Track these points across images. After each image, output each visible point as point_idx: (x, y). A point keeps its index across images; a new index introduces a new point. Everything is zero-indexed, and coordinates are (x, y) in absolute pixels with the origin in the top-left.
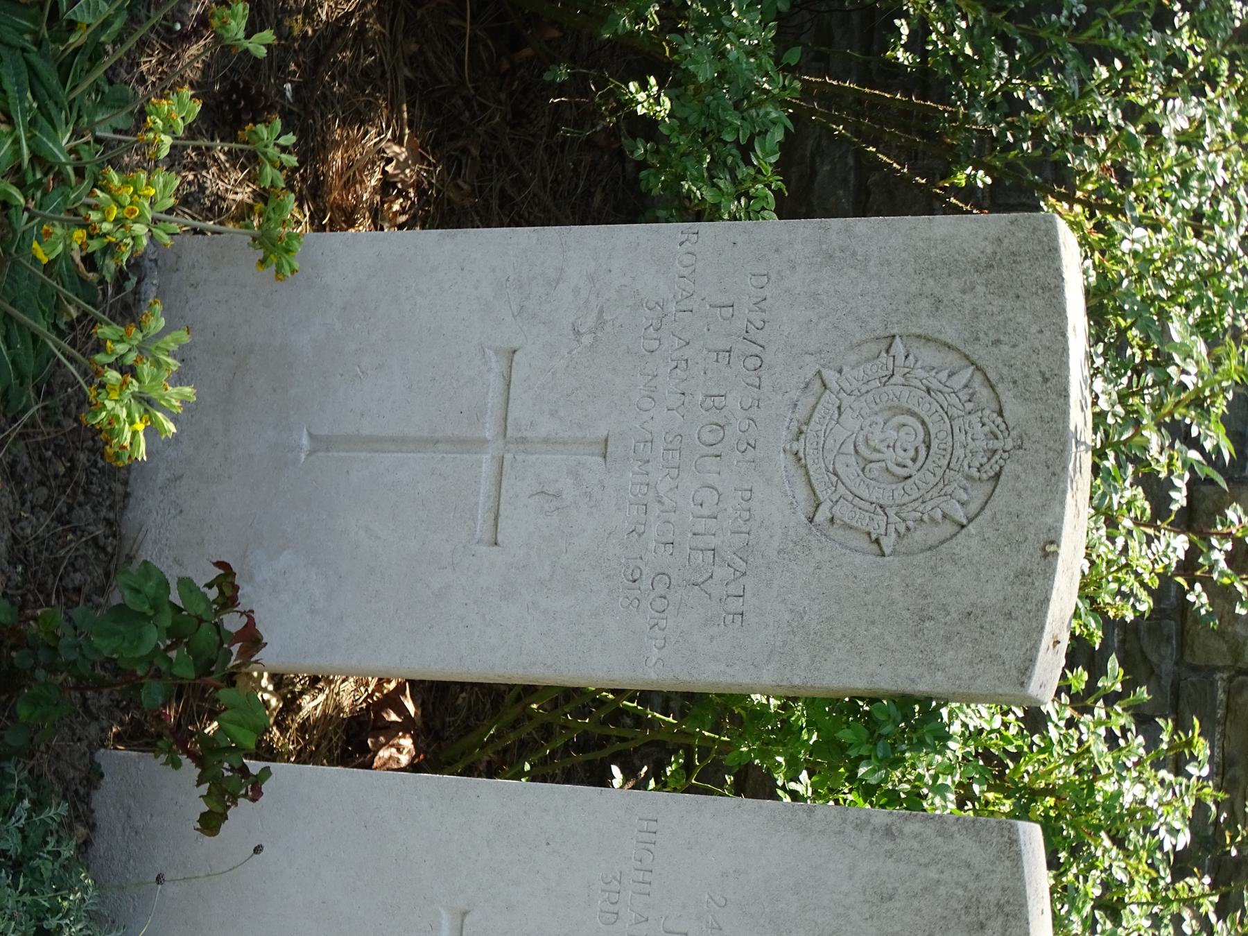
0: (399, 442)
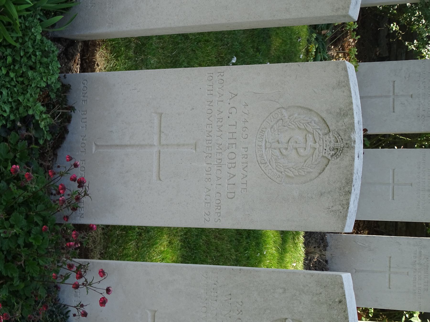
0: (376, 97)
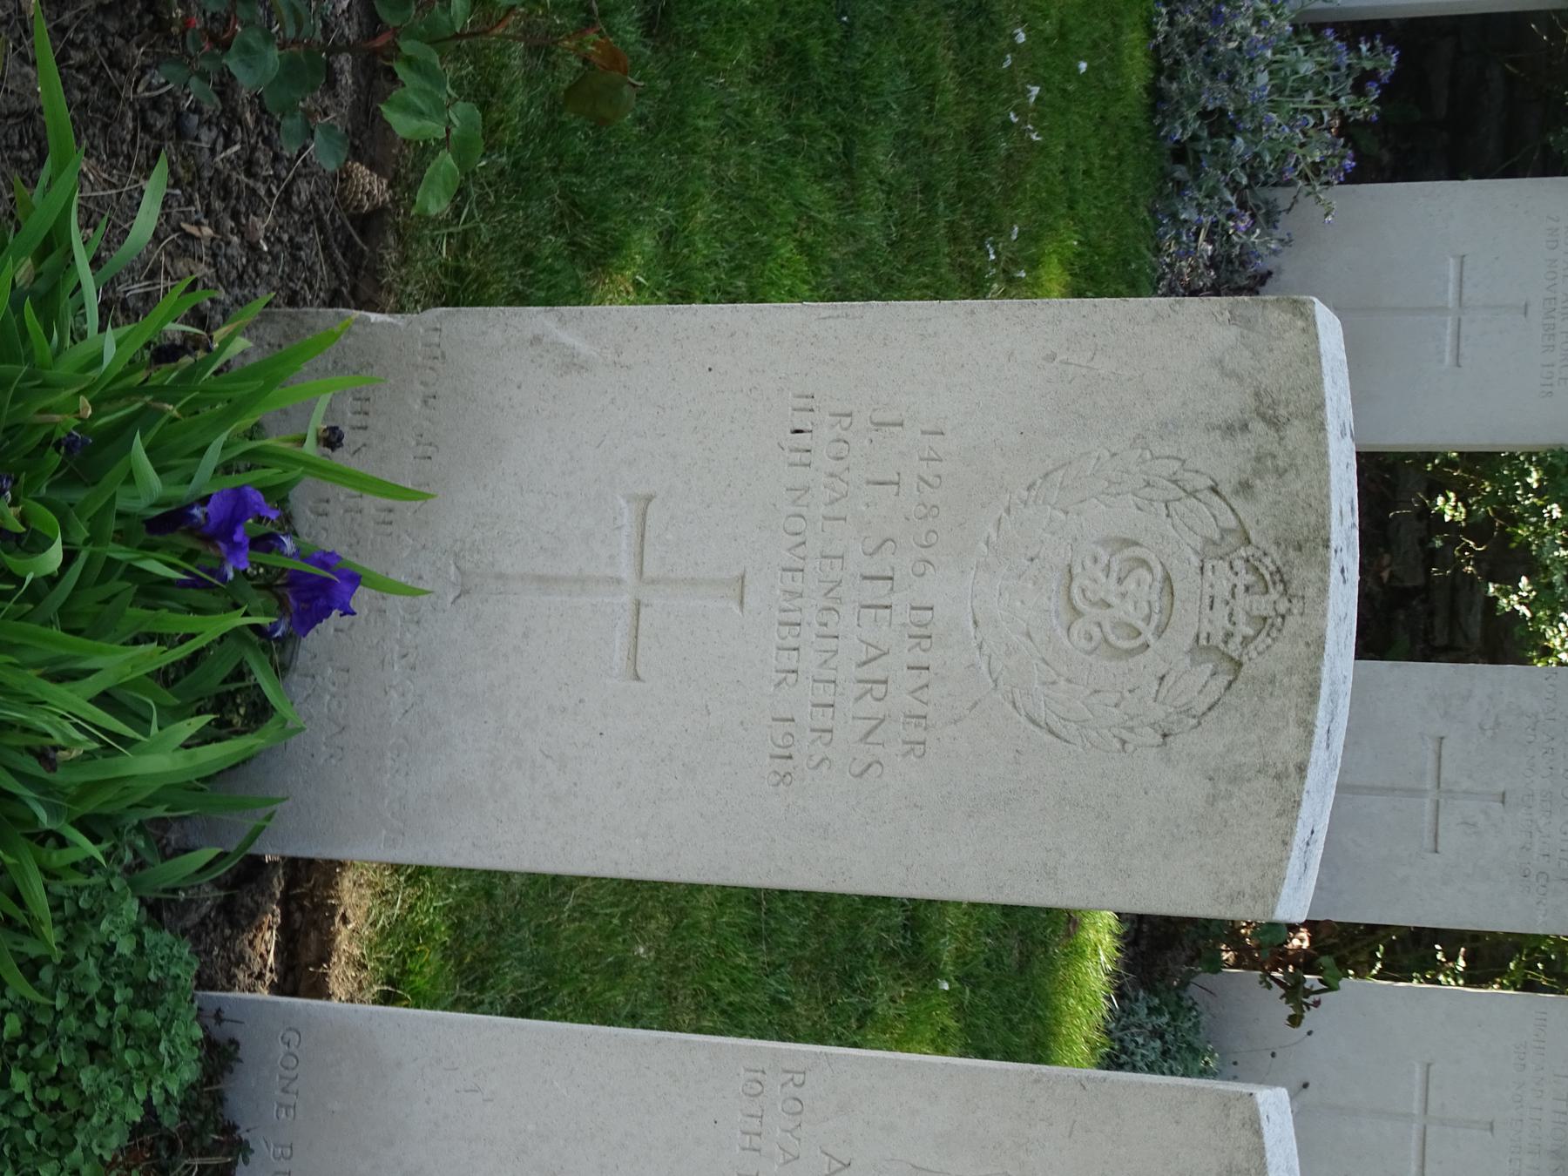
0: (1371, 790)
